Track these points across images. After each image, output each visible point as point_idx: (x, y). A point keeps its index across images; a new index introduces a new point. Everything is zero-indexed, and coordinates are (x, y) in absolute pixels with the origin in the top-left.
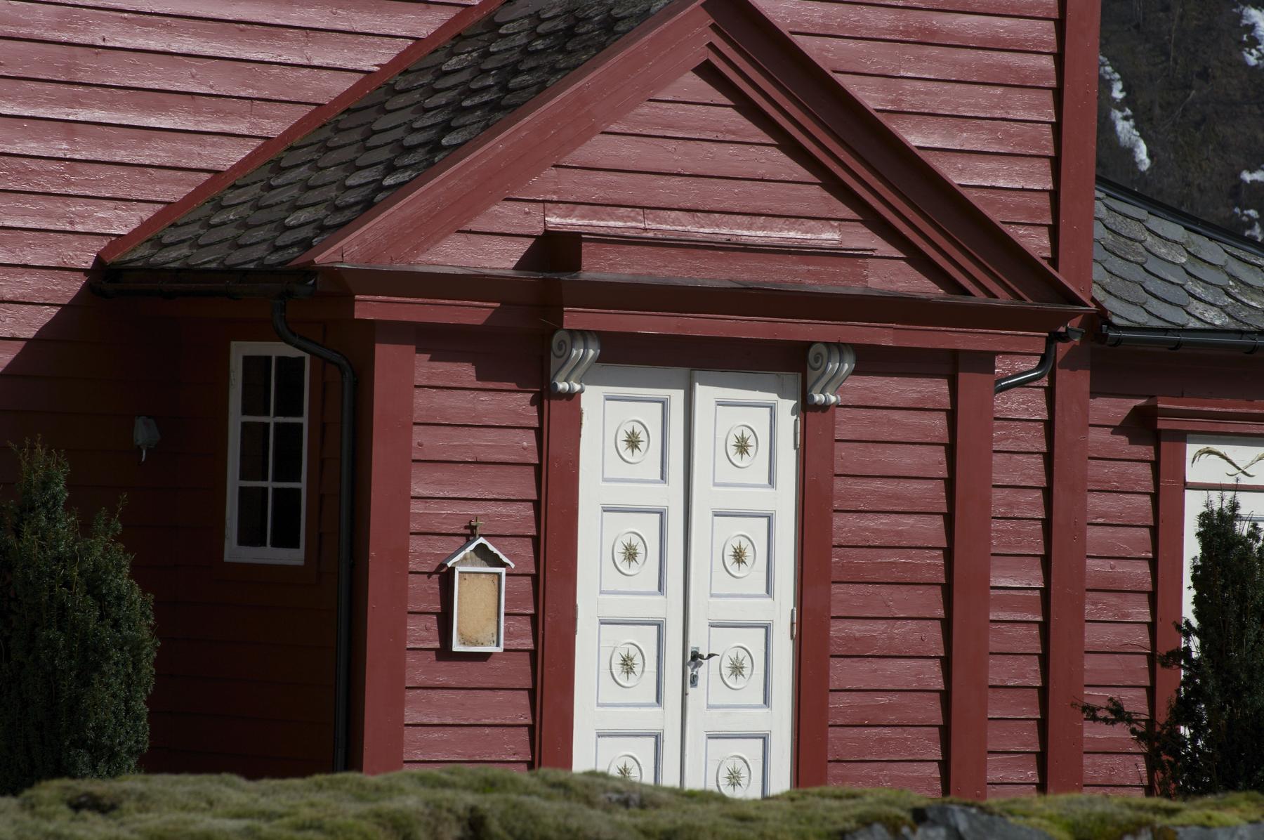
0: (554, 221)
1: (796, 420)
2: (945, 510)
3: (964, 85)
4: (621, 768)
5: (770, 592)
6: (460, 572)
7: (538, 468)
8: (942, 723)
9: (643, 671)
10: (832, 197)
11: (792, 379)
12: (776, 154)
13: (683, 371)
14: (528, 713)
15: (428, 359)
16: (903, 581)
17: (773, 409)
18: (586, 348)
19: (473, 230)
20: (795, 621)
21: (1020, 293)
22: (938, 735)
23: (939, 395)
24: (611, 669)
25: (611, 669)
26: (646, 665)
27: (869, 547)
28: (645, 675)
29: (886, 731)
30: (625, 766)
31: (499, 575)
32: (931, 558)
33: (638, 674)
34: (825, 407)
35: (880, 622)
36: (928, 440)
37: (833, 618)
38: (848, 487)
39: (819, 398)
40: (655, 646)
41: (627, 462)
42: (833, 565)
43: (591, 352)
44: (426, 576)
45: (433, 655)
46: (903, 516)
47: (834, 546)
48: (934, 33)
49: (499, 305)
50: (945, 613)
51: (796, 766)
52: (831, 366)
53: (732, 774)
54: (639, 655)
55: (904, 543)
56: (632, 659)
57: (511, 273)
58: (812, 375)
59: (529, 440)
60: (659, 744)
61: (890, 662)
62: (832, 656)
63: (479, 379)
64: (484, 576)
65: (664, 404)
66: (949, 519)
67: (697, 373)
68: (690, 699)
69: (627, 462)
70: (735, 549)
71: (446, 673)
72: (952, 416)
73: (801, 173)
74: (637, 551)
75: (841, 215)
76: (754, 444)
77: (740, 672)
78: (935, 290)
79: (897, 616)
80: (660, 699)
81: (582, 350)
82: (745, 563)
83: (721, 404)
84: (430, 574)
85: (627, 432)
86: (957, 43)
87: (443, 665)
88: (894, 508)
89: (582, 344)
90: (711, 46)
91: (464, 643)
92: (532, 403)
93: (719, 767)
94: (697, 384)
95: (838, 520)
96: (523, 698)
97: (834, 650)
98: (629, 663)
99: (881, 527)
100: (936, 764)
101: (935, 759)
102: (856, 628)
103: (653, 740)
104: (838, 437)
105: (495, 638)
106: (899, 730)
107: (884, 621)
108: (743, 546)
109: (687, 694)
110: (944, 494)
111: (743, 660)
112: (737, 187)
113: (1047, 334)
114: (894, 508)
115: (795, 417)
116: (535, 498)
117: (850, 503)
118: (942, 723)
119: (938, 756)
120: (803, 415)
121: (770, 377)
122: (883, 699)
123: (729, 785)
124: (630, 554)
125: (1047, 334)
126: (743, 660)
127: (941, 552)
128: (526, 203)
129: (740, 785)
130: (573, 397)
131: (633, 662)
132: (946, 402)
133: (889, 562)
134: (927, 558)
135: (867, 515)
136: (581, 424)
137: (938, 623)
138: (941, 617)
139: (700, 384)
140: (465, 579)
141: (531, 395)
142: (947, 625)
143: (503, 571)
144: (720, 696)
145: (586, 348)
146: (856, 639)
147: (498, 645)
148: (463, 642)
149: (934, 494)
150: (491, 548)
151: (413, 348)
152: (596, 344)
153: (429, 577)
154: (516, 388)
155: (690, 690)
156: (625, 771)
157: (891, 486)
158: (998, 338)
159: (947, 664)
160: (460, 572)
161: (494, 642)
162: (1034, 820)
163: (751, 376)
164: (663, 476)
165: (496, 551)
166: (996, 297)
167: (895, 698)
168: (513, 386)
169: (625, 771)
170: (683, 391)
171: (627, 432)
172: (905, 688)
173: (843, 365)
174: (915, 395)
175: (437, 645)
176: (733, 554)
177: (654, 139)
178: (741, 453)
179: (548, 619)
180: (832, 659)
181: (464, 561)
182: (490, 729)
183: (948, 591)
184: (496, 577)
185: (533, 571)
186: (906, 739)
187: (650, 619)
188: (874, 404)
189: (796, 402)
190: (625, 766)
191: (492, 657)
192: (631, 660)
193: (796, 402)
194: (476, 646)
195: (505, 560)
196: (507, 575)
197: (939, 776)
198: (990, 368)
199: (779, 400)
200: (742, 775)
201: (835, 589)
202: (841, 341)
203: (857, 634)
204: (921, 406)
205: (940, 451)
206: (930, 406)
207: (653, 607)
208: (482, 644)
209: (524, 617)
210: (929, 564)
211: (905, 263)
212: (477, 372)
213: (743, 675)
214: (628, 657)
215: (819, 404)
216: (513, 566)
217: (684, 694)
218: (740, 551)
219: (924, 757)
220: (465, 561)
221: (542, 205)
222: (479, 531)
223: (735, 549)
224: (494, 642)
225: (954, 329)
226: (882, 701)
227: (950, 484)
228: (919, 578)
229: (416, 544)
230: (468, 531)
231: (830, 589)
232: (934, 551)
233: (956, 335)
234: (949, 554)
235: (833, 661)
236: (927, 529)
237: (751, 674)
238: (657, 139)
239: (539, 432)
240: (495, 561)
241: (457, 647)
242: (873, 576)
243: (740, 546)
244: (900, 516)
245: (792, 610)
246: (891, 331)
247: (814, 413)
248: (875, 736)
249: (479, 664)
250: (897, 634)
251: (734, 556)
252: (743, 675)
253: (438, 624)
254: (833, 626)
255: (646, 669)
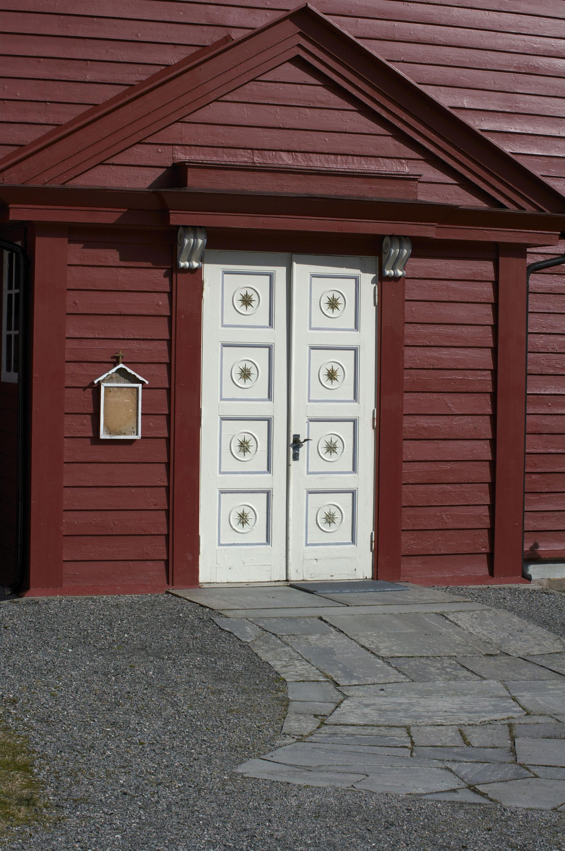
0: (181, 156)
1: (375, 287)
2: (492, 345)
3: (560, 99)
4: (239, 513)
5: (356, 398)
6: (105, 387)
7: (170, 318)
8: (490, 481)
9: (256, 450)
10: (401, 144)
11: (372, 260)
12: (357, 116)
13: (286, 255)
14: (165, 479)
15: (82, 247)
16: (461, 390)
17: (357, 280)
18: (401, 248)
19: (115, 163)
20: (375, 417)
21: (541, 207)
22: (488, 489)
23: (486, 272)
24: (231, 449)
25: (231, 449)
26: (259, 447)
27: (434, 369)
28: (257, 453)
29: (448, 487)
30: (243, 512)
31: (137, 388)
32: (482, 376)
33: (253, 453)
34: (396, 279)
35: (443, 417)
36: (478, 300)
37: (405, 415)
38: (417, 330)
39: (388, 272)
40: (266, 435)
41: (240, 313)
42: (405, 381)
43: (405, 251)
44: (82, 389)
45: (88, 441)
46: (460, 349)
47: (406, 369)
48: (538, 68)
49: (125, 210)
50: (492, 410)
51: (377, 510)
52: (393, 251)
53: (327, 516)
54: (253, 440)
55: (460, 367)
56: (248, 442)
57: (147, 190)
58: (384, 257)
59: (163, 300)
60: (269, 497)
61: (452, 443)
62: (404, 440)
63: (121, 259)
64: (125, 389)
65: (271, 276)
66: (495, 351)
67: (294, 256)
68: (292, 468)
69: (240, 313)
70: (328, 371)
71: (98, 453)
72: (496, 284)
73: (379, 129)
74: (251, 372)
75: (406, 156)
76: (343, 303)
77: (333, 450)
78: (481, 205)
79: (456, 413)
80: (270, 469)
81: (192, 240)
82: (337, 380)
83: (314, 276)
84: (85, 388)
85: (241, 295)
86: (554, 75)
87: (97, 447)
88: (453, 344)
89: (192, 235)
90: (299, 46)
91: (110, 433)
92: (165, 276)
93: (318, 512)
94: (294, 264)
95: (408, 352)
96: (162, 469)
97: (405, 435)
98: (246, 445)
99: (443, 356)
100: (487, 507)
101: (486, 503)
102: (423, 422)
103: (265, 495)
104: (407, 298)
105: (135, 430)
106: (458, 486)
107: (446, 417)
108: (335, 369)
109: (290, 465)
110: (491, 335)
111: (336, 443)
112: (327, 137)
113: (560, 233)
114: (453, 344)
115: (375, 285)
116: (168, 338)
117: (418, 341)
118: (490, 481)
119: (487, 501)
120: (380, 283)
121: (355, 259)
122: (448, 466)
123: (326, 523)
124: (245, 374)
125: (560, 233)
126: (336, 443)
127: (489, 372)
128: (160, 146)
129: (334, 523)
130: (197, 272)
131: (249, 445)
132: (491, 276)
133: (449, 379)
134: (479, 376)
135: (433, 348)
136: (203, 289)
137: (488, 417)
138: (490, 413)
139: (297, 263)
140: (110, 391)
141: (164, 271)
142: (494, 418)
143: (140, 386)
144: (317, 465)
145: (401, 248)
146: (424, 428)
147: (137, 434)
148: (109, 432)
149: (488, 338)
150: (129, 370)
151: (67, 239)
152: (204, 236)
153: (84, 391)
154: (152, 266)
155: (292, 462)
156: (243, 515)
157: (451, 330)
158: (521, 235)
159: (493, 443)
160: (105, 387)
161: (134, 432)
162: (266, 726)
163: (339, 258)
164: (271, 324)
165: (133, 373)
166: (525, 209)
167: (455, 466)
168: (149, 264)
169: (243, 515)
170: (285, 268)
171: (241, 295)
172: (462, 459)
173: (403, 251)
174: (467, 272)
175: (91, 435)
176: (327, 374)
177: (261, 106)
178: (333, 308)
179: (177, 417)
180: (404, 442)
181: (110, 379)
182: (135, 489)
183: (494, 396)
184: (135, 390)
185: (167, 386)
186: (463, 491)
187: (261, 417)
188: (435, 277)
189: (375, 275)
190: (243, 512)
191: (135, 442)
192: (247, 443)
193: (375, 275)
194: (119, 435)
195: (141, 378)
196: (142, 388)
197: (488, 514)
198: (524, 255)
199: (362, 274)
200: (335, 517)
201: (406, 396)
202: (395, 234)
203: (426, 425)
204: (472, 278)
205: (488, 308)
206: (480, 279)
207: (264, 409)
208: (125, 434)
209: (161, 416)
210: (480, 380)
211: (458, 187)
212: (120, 256)
213: (336, 453)
214: (244, 442)
215: (397, 277)
216: (147, 382)
217: (288, 465)
218: (333, 372)
219: (477, 503)
220: (111, 380)
221: (171, 147)
222: (121, 360)
223: (328, 371)
224: (134, 432)
225: (489, 229)
226: (444, 467)
227: (495, 328)
228: (471, 388)
229: (71, 368)
230: (114, 360)
231: (402, 396)
232: (484, 371)
233: (490, 232)
234: (494, 373)
235: (405, 443)
236: (479, 357)
237: (343, 452)
238: (263, 106)
239: (170, 294)
240: (134, 379)
241: (103, 436)
242: (437, 388)
243: (332, 369)
244: (458, 349)
245: (374, 410)
246: (434, 228)
247: (388, 282)
248: (439, 490)
249: (126, 447)
250: (456, 425)
251: (327, 375)
252: (336, 453)
253: (92, 421)
254: (406, 420)
255: (258, 450)
